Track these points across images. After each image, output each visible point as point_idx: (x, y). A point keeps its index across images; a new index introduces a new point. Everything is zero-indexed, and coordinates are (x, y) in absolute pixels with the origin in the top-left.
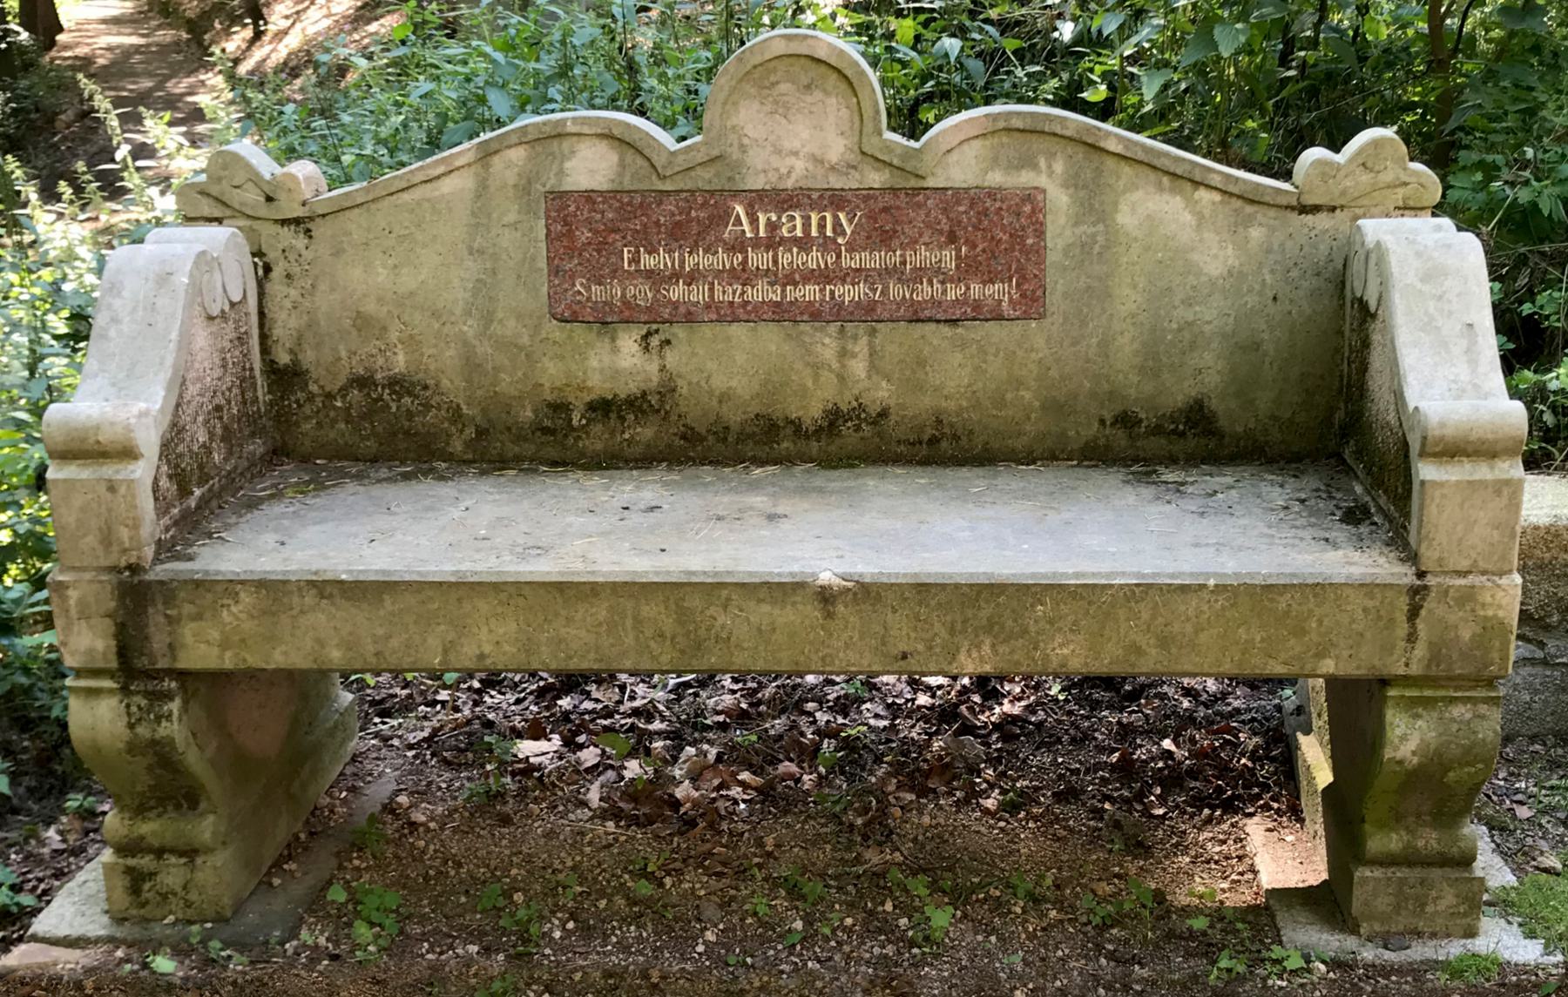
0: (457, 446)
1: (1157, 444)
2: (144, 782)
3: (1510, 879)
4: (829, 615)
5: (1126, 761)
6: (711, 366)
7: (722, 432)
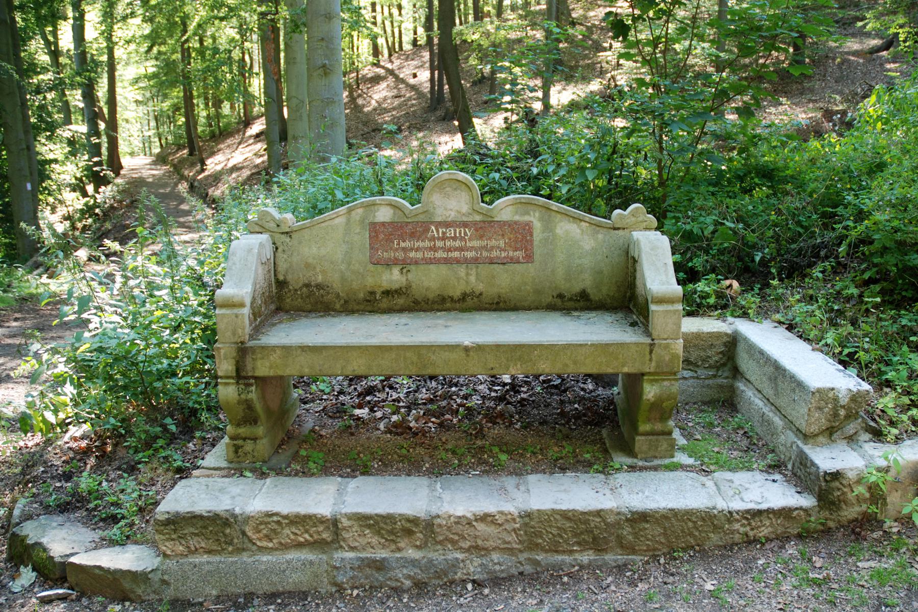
0: (338, 306)
1: (570, 304)
2: (241, 414)
3: (686, 442)
4: (468, 356)
5: (562, 411)
6: (424, 278)
7: (427, 301)
